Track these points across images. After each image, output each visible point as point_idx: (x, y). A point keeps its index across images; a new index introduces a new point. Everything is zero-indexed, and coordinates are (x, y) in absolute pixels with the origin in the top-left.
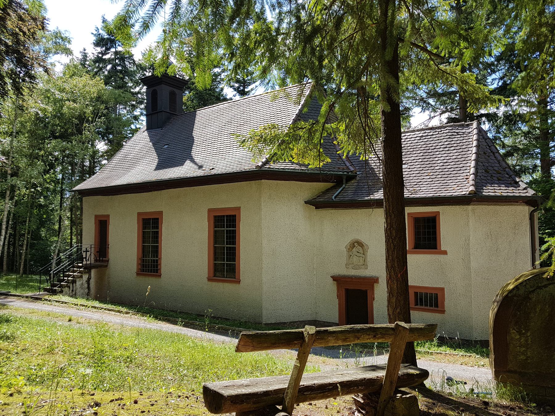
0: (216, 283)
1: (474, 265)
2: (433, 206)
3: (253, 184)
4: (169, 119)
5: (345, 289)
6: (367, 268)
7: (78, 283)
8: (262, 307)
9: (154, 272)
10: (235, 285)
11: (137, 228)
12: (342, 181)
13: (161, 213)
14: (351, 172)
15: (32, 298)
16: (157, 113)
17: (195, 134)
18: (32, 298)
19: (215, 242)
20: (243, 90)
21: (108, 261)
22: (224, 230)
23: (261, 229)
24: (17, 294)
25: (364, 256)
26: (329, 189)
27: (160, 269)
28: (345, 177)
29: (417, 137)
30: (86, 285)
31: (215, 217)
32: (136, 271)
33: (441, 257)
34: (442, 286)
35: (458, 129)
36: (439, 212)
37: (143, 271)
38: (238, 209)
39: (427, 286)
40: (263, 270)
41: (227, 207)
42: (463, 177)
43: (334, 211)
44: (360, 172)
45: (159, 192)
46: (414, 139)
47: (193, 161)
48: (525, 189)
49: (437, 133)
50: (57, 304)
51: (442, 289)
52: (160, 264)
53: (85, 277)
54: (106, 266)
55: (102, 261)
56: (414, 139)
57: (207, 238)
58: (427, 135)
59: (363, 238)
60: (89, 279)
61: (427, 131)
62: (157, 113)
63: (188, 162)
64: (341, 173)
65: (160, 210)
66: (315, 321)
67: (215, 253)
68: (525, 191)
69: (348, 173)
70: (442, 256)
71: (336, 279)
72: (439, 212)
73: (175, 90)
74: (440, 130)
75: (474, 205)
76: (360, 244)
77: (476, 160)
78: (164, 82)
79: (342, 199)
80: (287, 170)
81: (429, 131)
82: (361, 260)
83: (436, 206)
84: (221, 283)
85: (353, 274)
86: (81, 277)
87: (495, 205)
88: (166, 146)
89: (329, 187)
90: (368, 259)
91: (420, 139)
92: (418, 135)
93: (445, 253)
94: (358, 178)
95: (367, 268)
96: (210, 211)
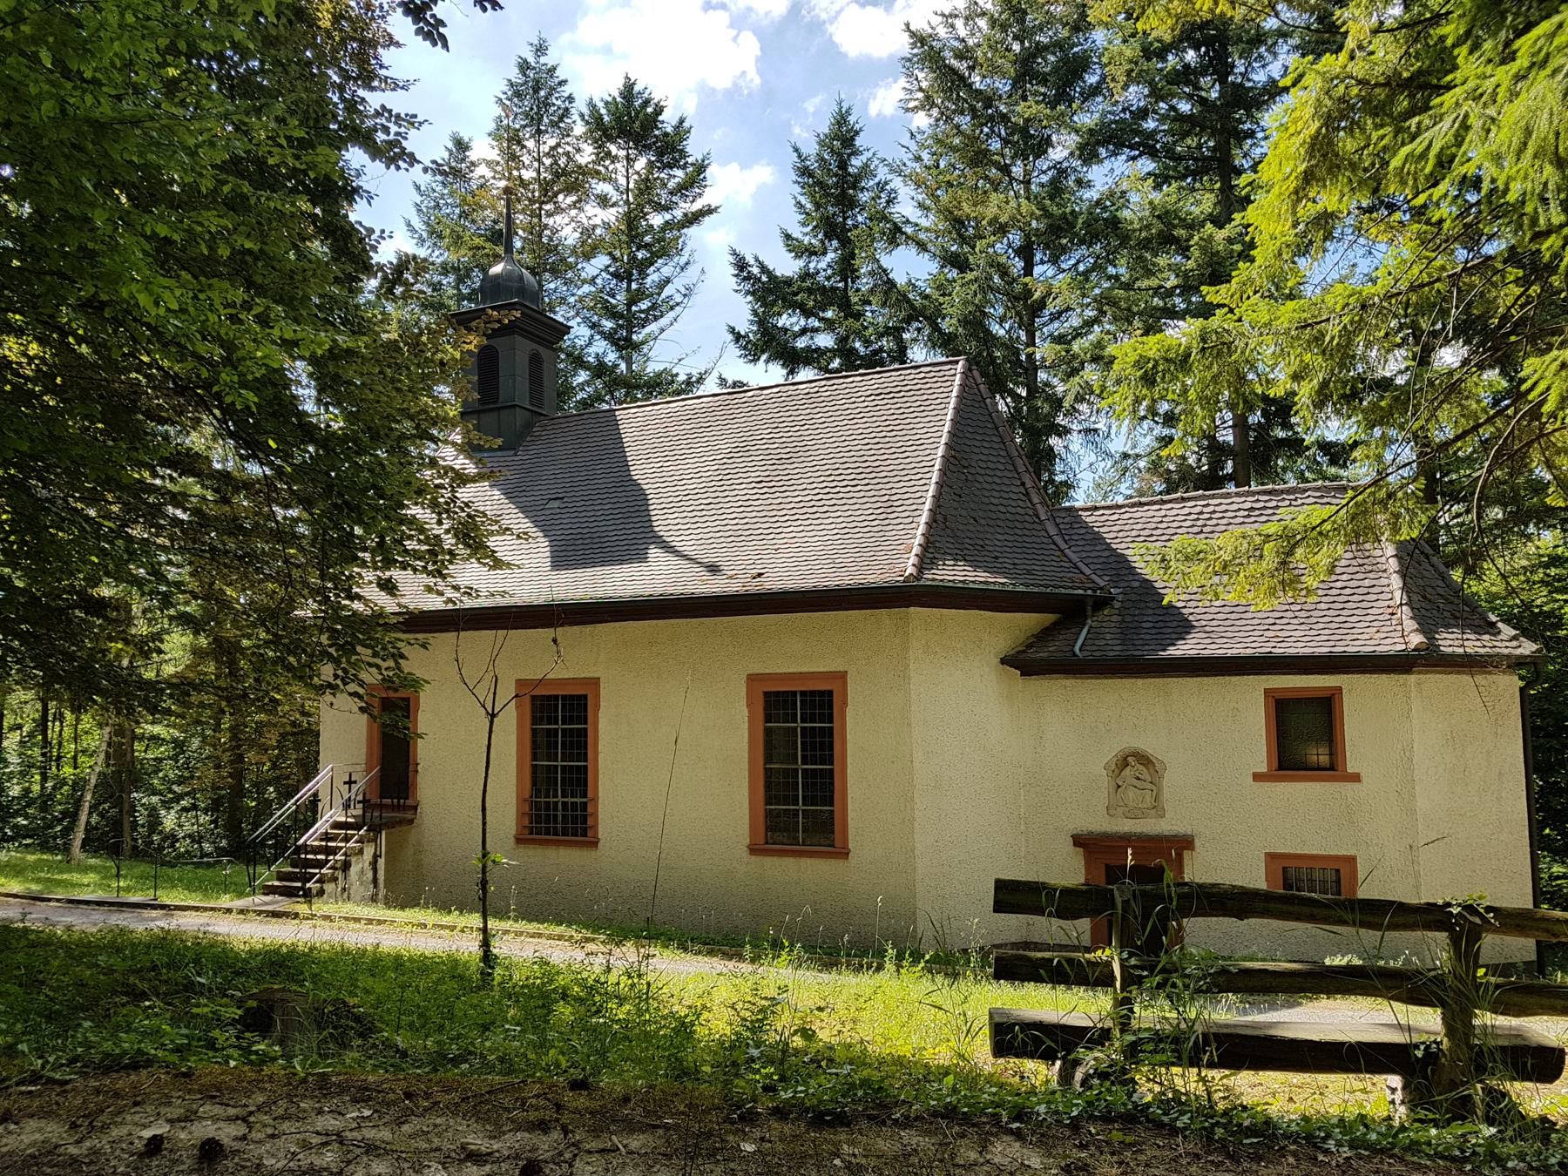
0: (775, 859)
1: (1422, 804)
2: (1326, 673)
3: (885, 617)
4: (529, 426)
5: (1107, 865)
6: (1163, 816)
7: (354, 870)
8: (914, 913)
9: (556, 834)
10: (833, 861)
11: (514, 722)
12: (1085, 610)
13: (595, 682)
14: (1101, 589)
15: (260, 913)
16: (498, 409)
17: (637, 473)
18: (260, 913)
19: (768, 758)
20: (628, 339)
21: (415, 808)
22: (796, 728)
23: (909, 725)
24: (192, 903)
25: (1154, 787)
26: (1047, 629)
27: (595, 827)
28: (1090, 602)
29: (1240, 509)
30: (370, 875)
31: (766, 694)
32: (514, 832)
33: (1347, 788)
34: (1351, 852)
35: (1334, 497)
36: (1340, 689)
37: (531, 833)
38: (842, 676)
39: (1314, 852)
40: (916, 824)
41: (805, 669)
42: (1381, 611)
43: (1073, 681)
44: (1119, 590)
45: (588, 629)
46: (1234, 514)
47: (668, 548)
48: (1514, 638)
49: (1288, 503)
50: (352, 925)
51: (1352, 860)
52: (595, 814)
53: (369, 851)
54: (411, 822)
55: (399, 808)
56: (1234, 514)
57: (746, 747)
58: (1265, 508)
59: (1147, 745)
60: (376, 857)
61: (1261, 498)
62: (498, 409)
63: (654, 552)
64: (1081, 592)
65: (591, 675)
66: (1026, 943)
67: (768, 786)
68: (1514, 643)
69: (1095, 591)
70: (1349, 785)
71: (1079, 841)
72: (1340, 689)
73: (541, 349)
74: (1292, 497)
75: (1420, 673)
76: (1144, 760)
77: (1403, 574)
78: (522, 329)
79: (1097, 654)
80: (971, 586)
81: (1267, 498)
82: (1148, 798)
83: (1332, 673)
84: (792, 860)
85: (1126, 829)
86: (361, 852)
87: (1458, 673)
88: (556, 504)
89: (1047, 624)
90: (1166, 794)
91: (1249, 516)
92: (1240, 506)
93: (1356, 778)
94: (1117, 605)
95: (1163, 816)
96: (752, 679)
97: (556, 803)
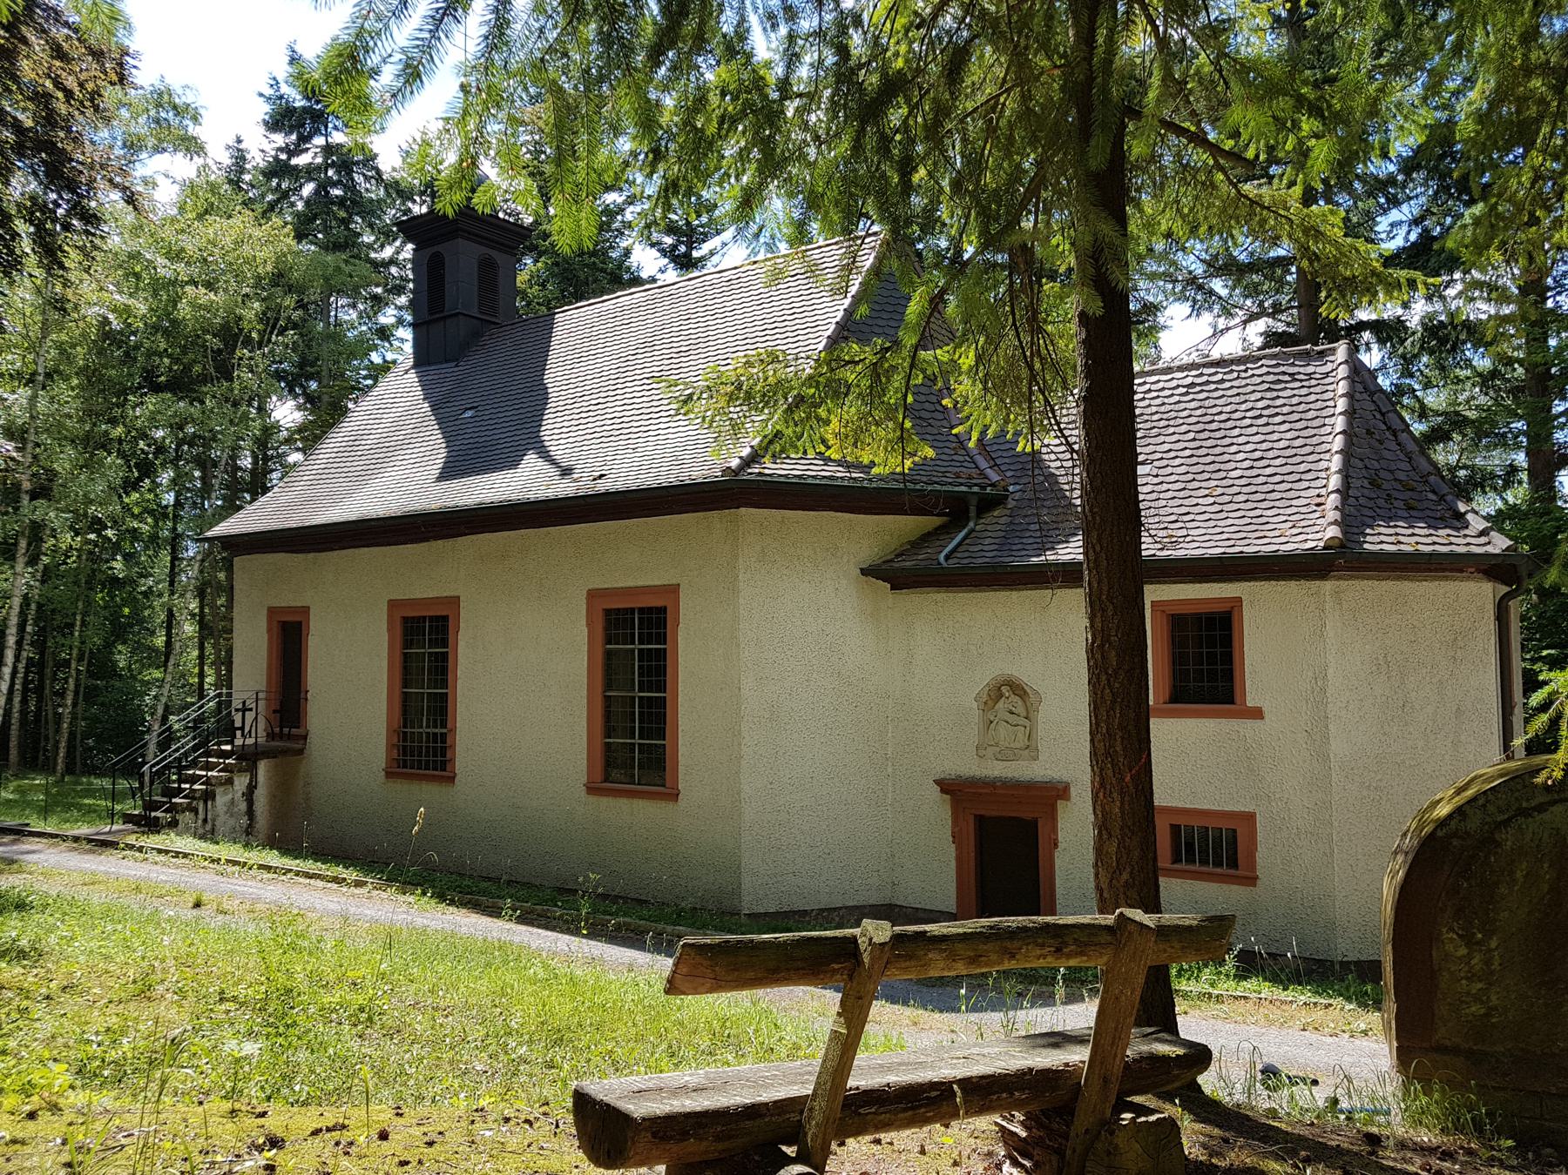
0: (610, 799)
1: (1338, 747)
2: (1224, 581)
3: (716, 519)
4: (476, 335)
5: (976, 816)
6: (1036, 758)
7: (222, 799)
8: (739, 867)
9: (435, 769)
10: (663, 804)
11: (386, 645)
12: (967, 511)
13: (455, 601)
14: (993, 485)
15: (90, 841)
16: (445, 318)
17: (550, 378)
18: (90, 841)
19: (609, 684)
20: (687, 255)
21: (305, 738)
22: (633, 650)
23: (738, 646)
24: (49, 830)
25: (1027, 723)
26: (929, 534)
27: (452, 760)
28: (974, 501)
29: (1178, 386)
30: (243, 806)
31: (608, 612)
32: (384, 765)
33: (1246, 727)
34: (1249, 808)
35: (1293, 364)
36: (1239, 600)
37: (405, 766)
38: (674, 590)
39: (1205, 807)
40: (743, 762)
41: (640, 583)
42: (1308, 501)
43: (944, 595)
44: (1018, 487)
45: (449, 543)
46: (1170, 392)
47: (545, 454)
48: (1483, 533)
49: (1235, 374)
50: (162, 858)
51: (1250, 818)
52: (453, 746)
53: (241, 782)
54: (301, 752)
55: (290, 737)
56: (1170, 392)
57: (585, 673)
58: (1208, 383)
59: (1024, 672)
60: (252, 788)
61: (1206, 371)
62: (445, 318)
63: (531, 459)
64: (963, 489)
65: (452, 594)
66: (891, 907)
67: (608, 715)
68: (1483, 540)
69: (984, 488)
70: (1249, 723)
71: (949, 787)
72: (1239, 600)
73: (494, 253)
74: (1243, 368)
75: (1340, 578)
76: (1018, 689)
77: (1346, 453)
78: (465, 231)
79: (966, 561)
80: (810, 481)
81: (1213, 370)
82: (1020, 735)
83: (1231, 581)
84: (625, 801)
85: (996, 773)
86: (230, 782)
87: (1398, 578)
88: (469, 414)
89: (930, 528)
90: (1041, 731)
91: (1187, 393)
92: (1180, 382)
93: (1257, 714)
94: (1011, 504)
95: (1036, 758)
96: (593, 595)
97: (428, 727)
